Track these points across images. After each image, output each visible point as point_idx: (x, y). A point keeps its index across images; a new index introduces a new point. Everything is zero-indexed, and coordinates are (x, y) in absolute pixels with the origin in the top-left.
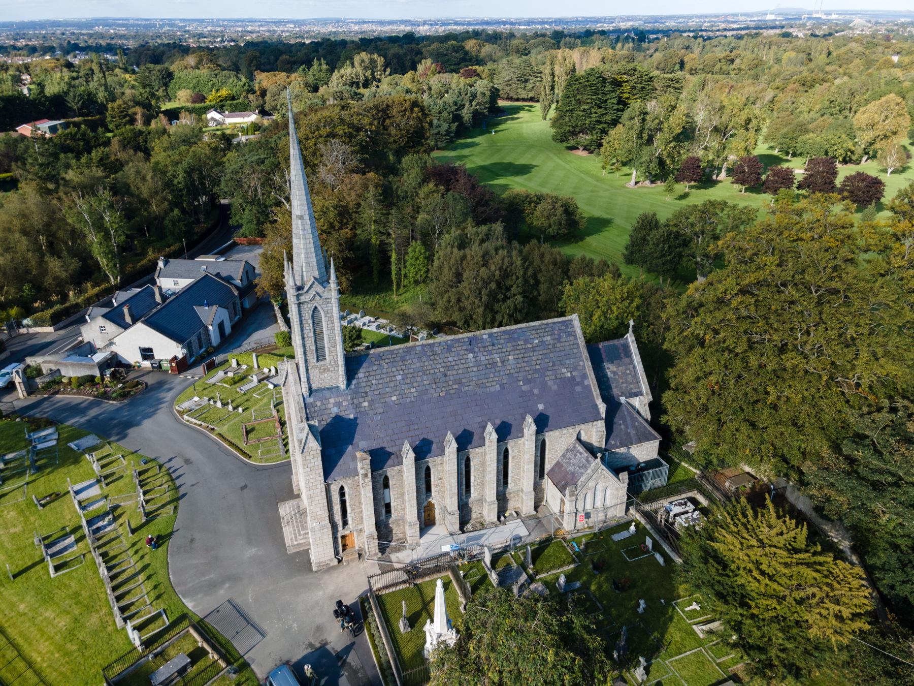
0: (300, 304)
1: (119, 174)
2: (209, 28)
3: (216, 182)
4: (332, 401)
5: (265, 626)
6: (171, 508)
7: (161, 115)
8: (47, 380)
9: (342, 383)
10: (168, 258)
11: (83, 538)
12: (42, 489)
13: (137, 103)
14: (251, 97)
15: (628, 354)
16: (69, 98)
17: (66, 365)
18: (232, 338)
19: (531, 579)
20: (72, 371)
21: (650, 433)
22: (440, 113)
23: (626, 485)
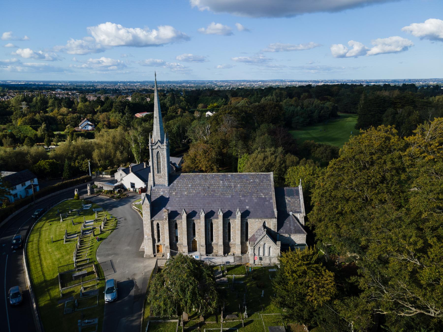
0: (152, 149)
5: (117, 270)
6: (110, 231)
8: (98, 190)
15: (298, 194)
17: (105, 185)
19: (223, 276)
20: (107, 188)
23: (279, 248)
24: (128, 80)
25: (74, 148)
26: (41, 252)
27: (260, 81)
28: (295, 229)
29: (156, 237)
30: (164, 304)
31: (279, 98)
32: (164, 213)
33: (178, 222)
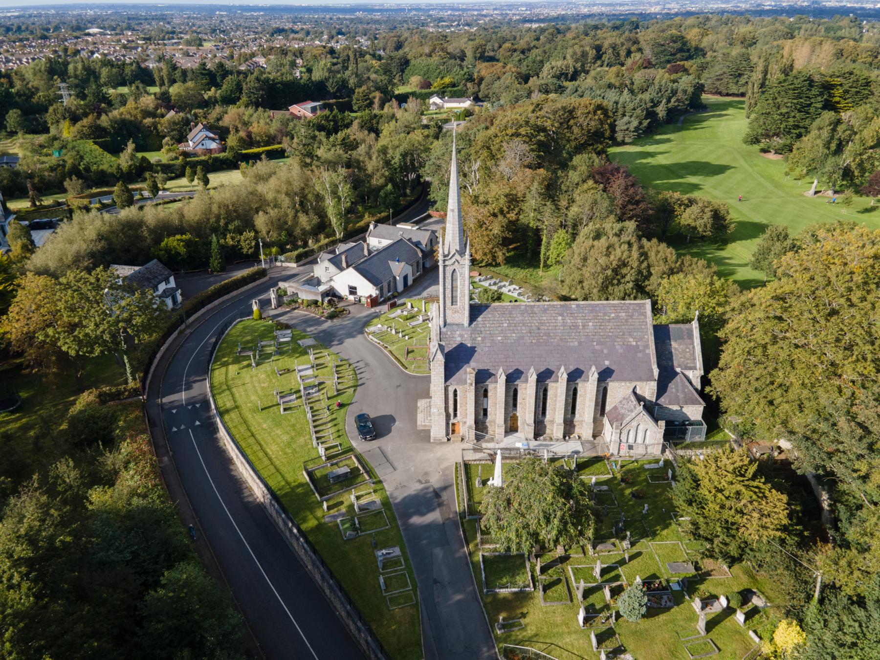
0: (445, 266)
1: (355, 152)
2: (449, 12)
3: (422, 165)
4: (458, 333)
5: (396, 464)
7: (393, 99)
9: (466, 321)
10: (379, 222)
11: (301, 397)
12: (280, 365)
13: (378, 88)
14: (469, 85)
16: (328, 84)
17: (301, 291)
18: (412, 287)
20: (306, 295)
21: (696, 399)
22: (634, 109)
23: (663, 431)
24: (237, 3)
25: (219, 207)
26: (253, 429)
27: (522, 5)
28: (685, 397)
29: (451, 410)
30: (517, 536)
31: (579, 64)
32: (468, 373)
33: (491, 387)
